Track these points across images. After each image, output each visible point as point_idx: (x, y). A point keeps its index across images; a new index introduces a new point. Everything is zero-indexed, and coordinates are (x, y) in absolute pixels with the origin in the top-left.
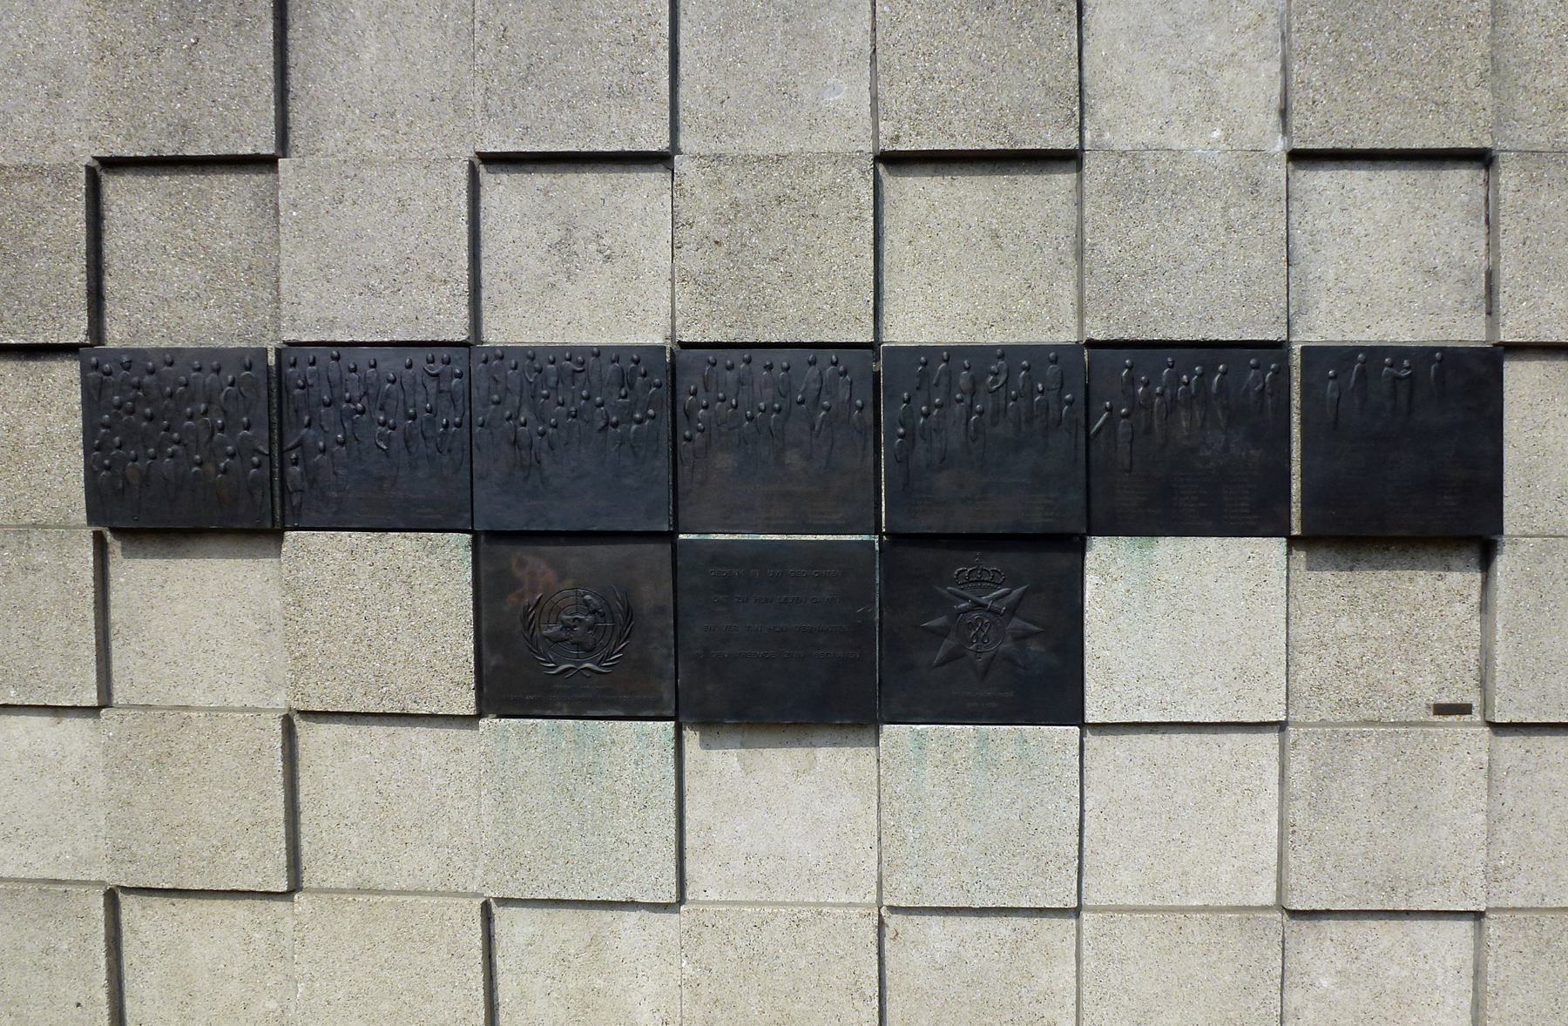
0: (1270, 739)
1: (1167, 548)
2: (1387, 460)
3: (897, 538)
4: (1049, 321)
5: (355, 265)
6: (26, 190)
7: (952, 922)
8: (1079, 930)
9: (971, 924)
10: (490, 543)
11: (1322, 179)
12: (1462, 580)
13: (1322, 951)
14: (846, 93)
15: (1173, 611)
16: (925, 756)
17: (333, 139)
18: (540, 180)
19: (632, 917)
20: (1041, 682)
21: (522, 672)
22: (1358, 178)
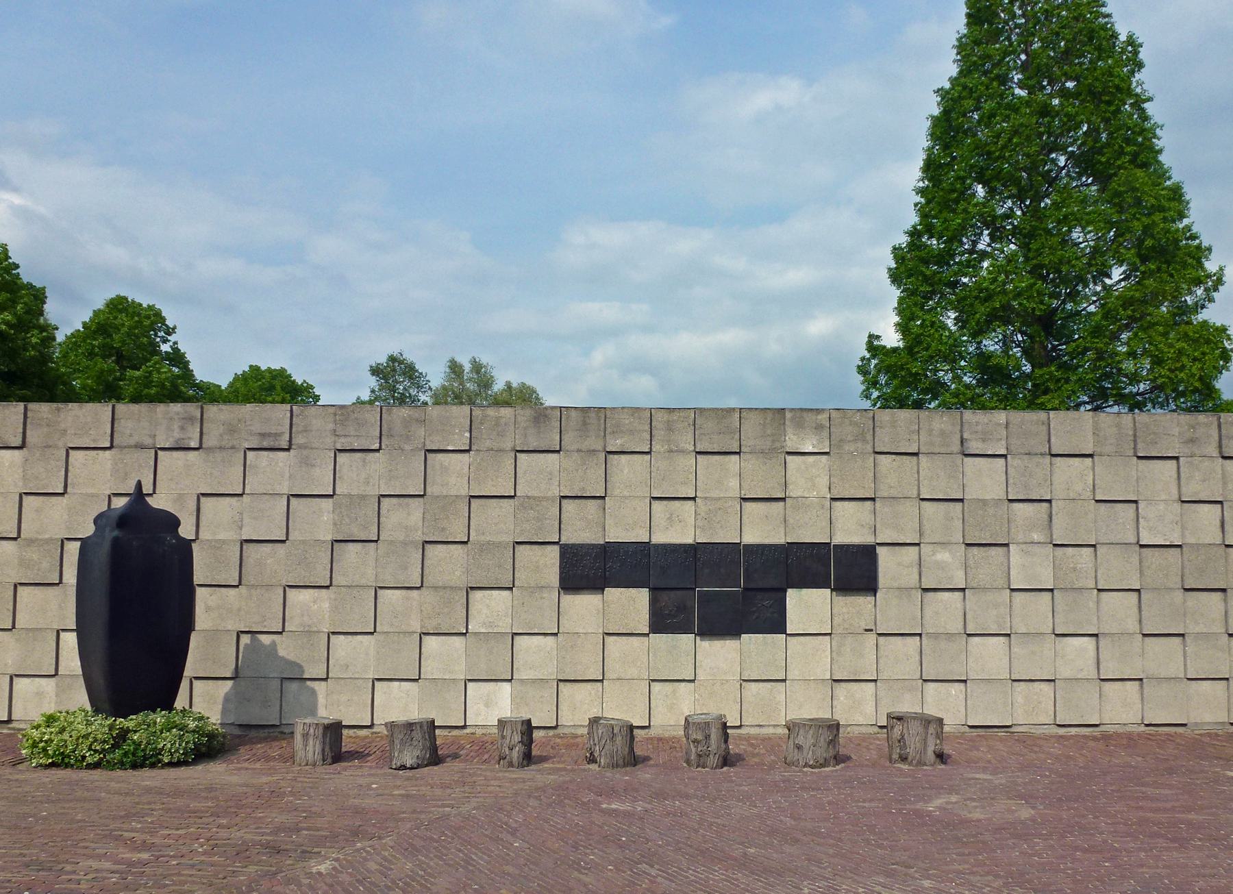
0: (828, 638)
1: (804, 591)
2: (853, 571)
3: (745, 589)
4: (778, 538)
5: (625, 526)
6: (544, 503)
7: (757, 684)
8: (1178, 468)
9: (761, 684)
10: (654, 590)
11: (838, 504)
12: (870, 599)
13: (841, 690)
14: (734, 483)
15: (806, 606)
16: (751, 641)
17: (617, 492)
18: (665, 502)
19: (683, 684)
20: (777, 624)
21: (661, 622)
22: (846, 503)
